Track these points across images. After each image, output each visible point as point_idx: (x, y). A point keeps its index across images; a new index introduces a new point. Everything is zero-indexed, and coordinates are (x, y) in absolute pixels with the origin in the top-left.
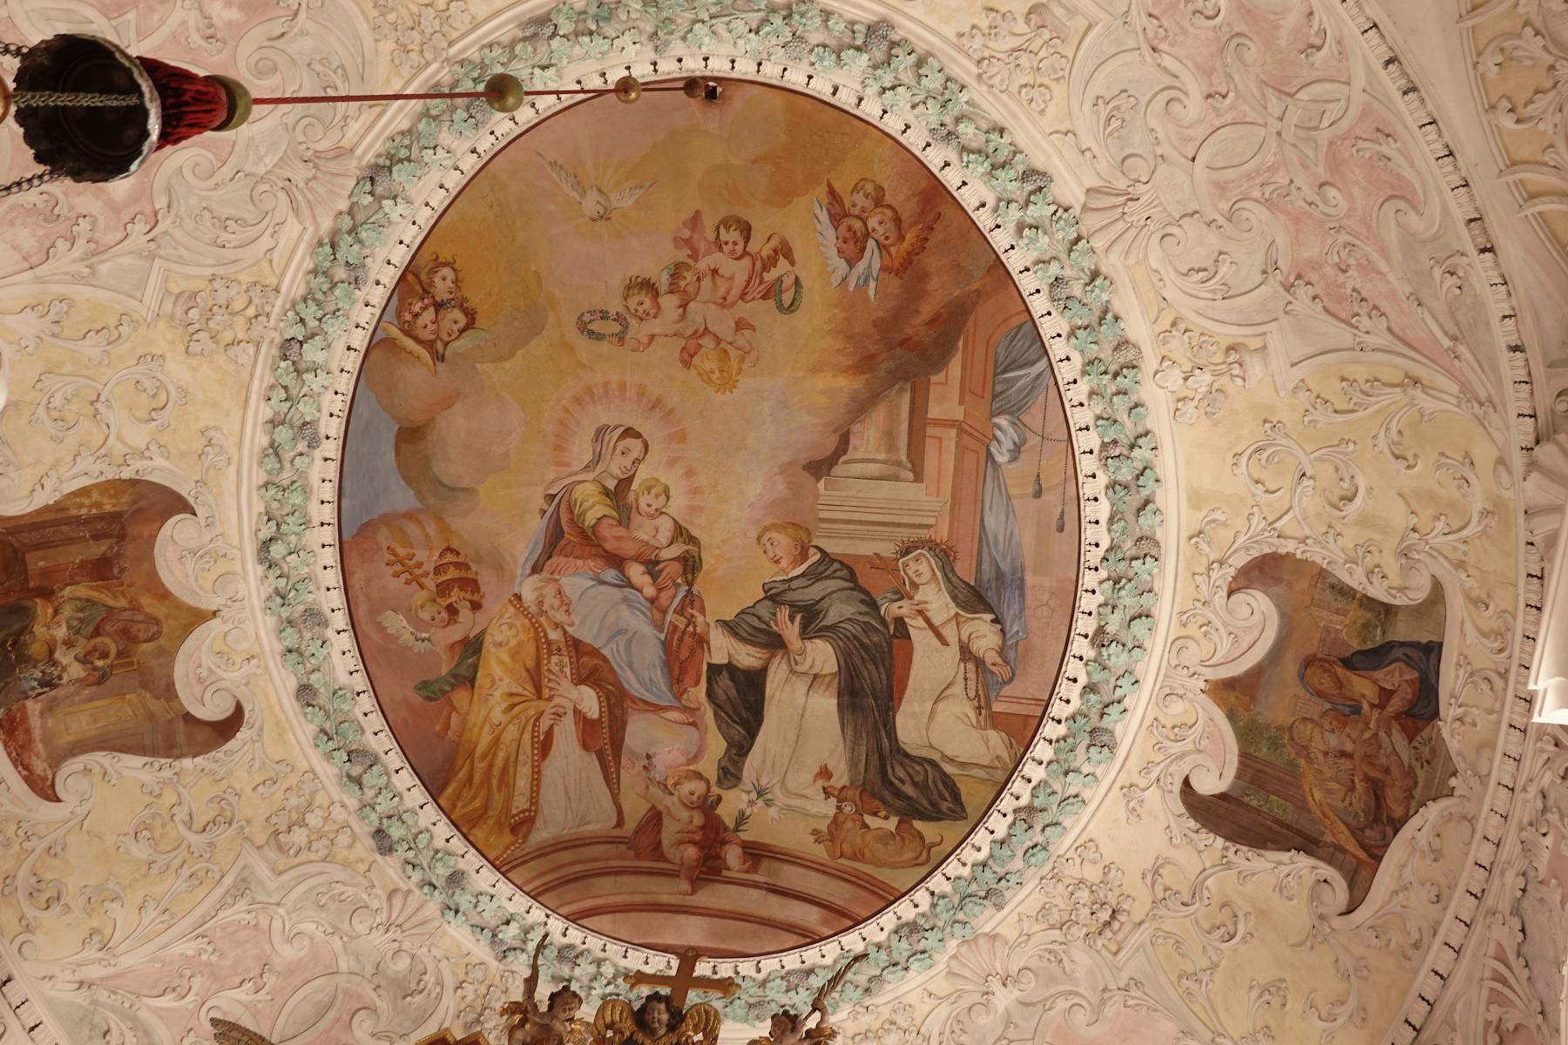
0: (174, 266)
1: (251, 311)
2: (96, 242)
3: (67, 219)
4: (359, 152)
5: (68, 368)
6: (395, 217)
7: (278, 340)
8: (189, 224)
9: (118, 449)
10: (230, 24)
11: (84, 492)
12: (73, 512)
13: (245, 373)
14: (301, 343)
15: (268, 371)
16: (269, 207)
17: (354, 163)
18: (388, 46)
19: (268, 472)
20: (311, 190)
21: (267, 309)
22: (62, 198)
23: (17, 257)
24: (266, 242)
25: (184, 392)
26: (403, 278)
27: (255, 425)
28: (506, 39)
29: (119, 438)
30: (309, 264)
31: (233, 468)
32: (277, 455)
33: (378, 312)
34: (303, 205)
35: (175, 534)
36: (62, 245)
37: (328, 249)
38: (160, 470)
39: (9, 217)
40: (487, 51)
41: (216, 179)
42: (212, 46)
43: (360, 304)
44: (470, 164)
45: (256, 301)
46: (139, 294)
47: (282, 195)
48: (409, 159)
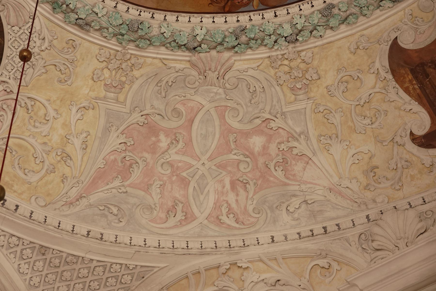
0: (283, 103)
1: (286, 62)
2: (288, 138)
3: (283, 154)
4: (188, 59)
5: (350, 123)
6: (204, 31)
7: (292, 45)
8: (261, 106)
9: (380, 85)
10: (167, 136)
11: (407, 91)
12: (418, 91)
13: (316, 50)
14: (286, 37)
15: (309, 42)
16: (235, 80)
17: (194, 58)
18: (136, 73)
19: (357, 18)
20: (216, 68)
21: (280, 57)
22: (274, 162)
23: (308, 167)
24: (251, 72)
25: (339, 70)
26: (230, 12)
27: (338, 34)
28: (98, 33)
29: (374, 87)
30: (249, 51)
31: (365, 32)
32: (346, 19)
33: (251, 14)
34: (225, 67)
35: (408, 42)
36: (295, 151)
37: (236, 49)
38: (382, 62)
39: (292, 178)
40: (108, 38)
41: (235, 106)
42: (179, 137)
43: (253, 22)
44: (159, 16)
45: (279, 63)
46: (303, 111)
47: (226, 77)
48: (175, 41)
